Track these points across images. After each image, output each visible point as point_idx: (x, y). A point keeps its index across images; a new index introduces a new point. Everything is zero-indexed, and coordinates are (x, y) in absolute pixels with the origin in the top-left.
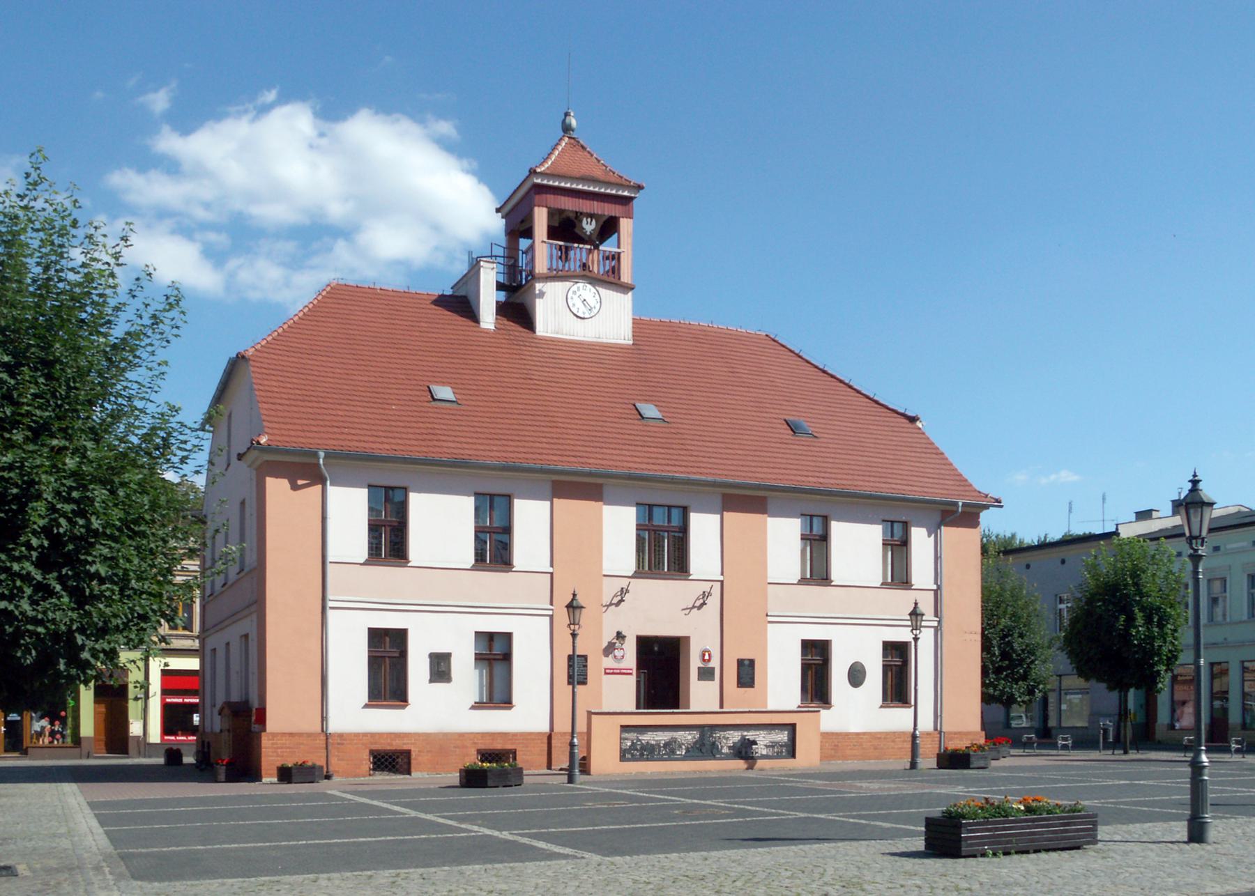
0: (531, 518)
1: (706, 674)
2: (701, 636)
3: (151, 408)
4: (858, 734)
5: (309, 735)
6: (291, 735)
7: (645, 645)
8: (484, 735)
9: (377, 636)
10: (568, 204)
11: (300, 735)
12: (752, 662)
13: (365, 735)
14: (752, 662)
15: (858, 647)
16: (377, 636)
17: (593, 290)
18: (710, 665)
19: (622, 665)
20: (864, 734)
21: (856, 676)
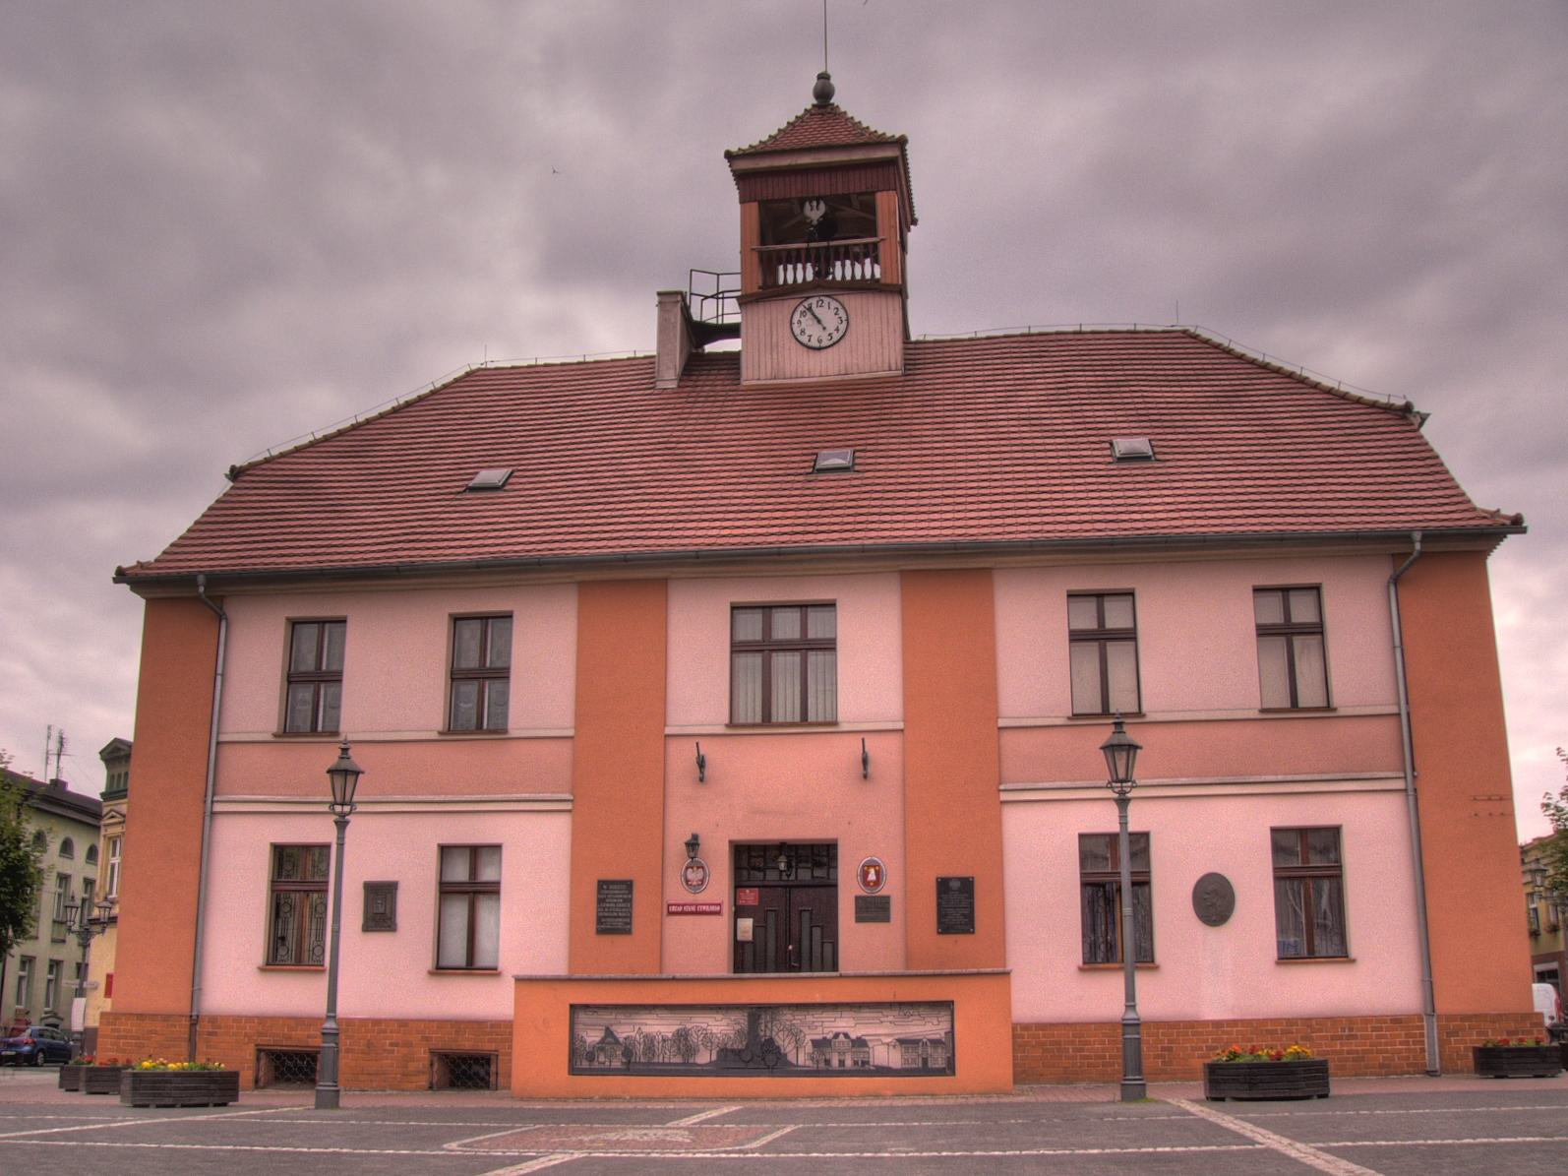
0: (545, 652)
1: (873, 909)
2: (871, 840)
3: (914, 1055)
4: (1218, 1024)
5: (166, 1017)
6: (141, 1016)
7: (749, 858)
8: (442, 1023)
9: (284, 857)
10: (840, 185)
11: (153, 1017)
12: (967, 885)
13: (250, 1019)
14: (967, 885)
15: (1207, 834)
16: (284, 857)
17: (834, 304)
18: (883, 891)
19: (701, 898)
20: (1234, 1023)
21: (1214, 901)
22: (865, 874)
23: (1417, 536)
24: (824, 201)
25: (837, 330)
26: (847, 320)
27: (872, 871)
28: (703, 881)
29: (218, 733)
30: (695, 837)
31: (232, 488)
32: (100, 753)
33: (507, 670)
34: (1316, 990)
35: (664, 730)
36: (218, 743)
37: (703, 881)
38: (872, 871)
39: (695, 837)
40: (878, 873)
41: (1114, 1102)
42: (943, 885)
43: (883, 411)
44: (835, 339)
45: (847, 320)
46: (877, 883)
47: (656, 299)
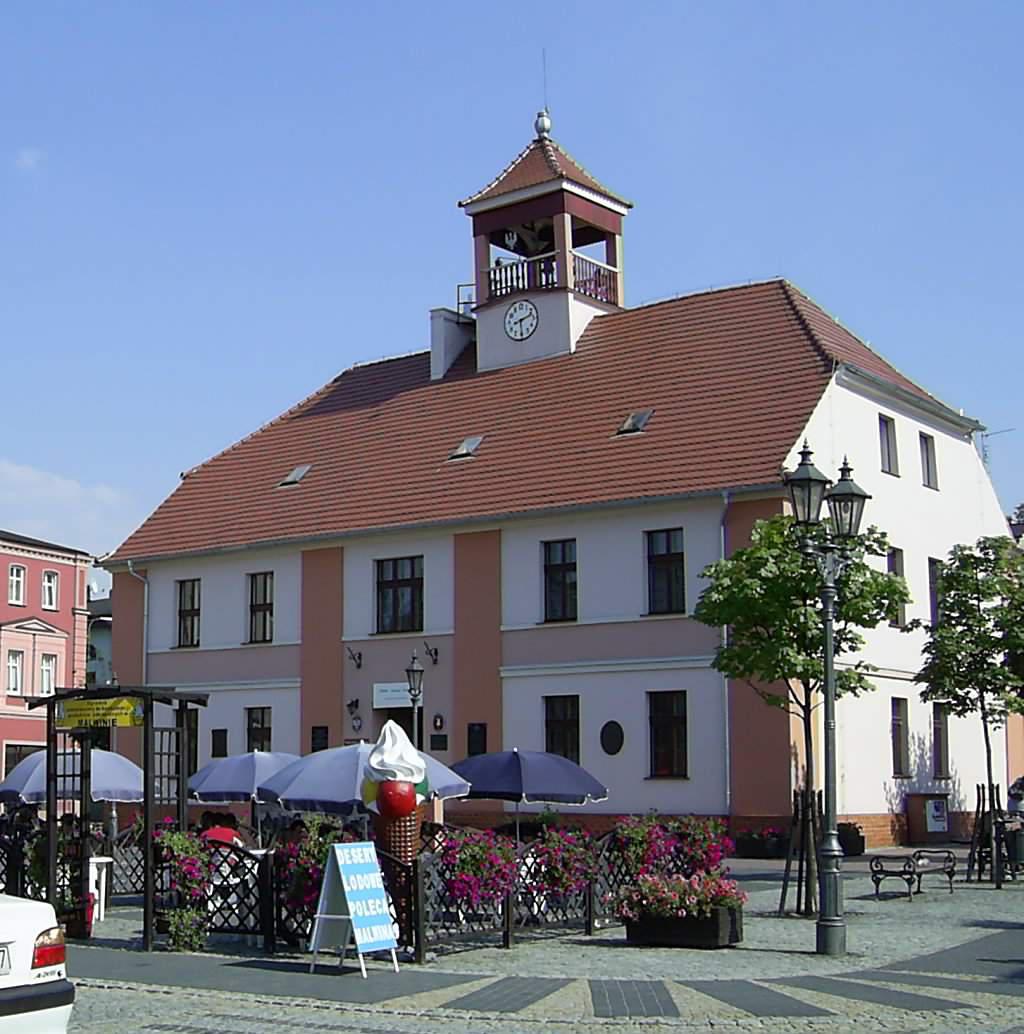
12: (483, 727)
14: (483, 727)
22: (435, 722)
23: (725, 494)
24: (530, 221)
25: (532, 325)
26: (537, 317)
27: (439, 721)
28: (360, 727)
29: (147, 649)
30: (357, 701)
31: (183, 484)
32: (874, 627)
33: (575, 564)
34: (668, 796)
35: (499, 628)
36: (147, 654)
37: (360, 727)
38: (439, 721)
39: (357, 701)
40: (441, 721)
41: (782, 913)
42: (471, 727)
43: (385, 456)
44: (531, 330)
45: (537, 317)
46: (441, 727)
47: (429, 314)
